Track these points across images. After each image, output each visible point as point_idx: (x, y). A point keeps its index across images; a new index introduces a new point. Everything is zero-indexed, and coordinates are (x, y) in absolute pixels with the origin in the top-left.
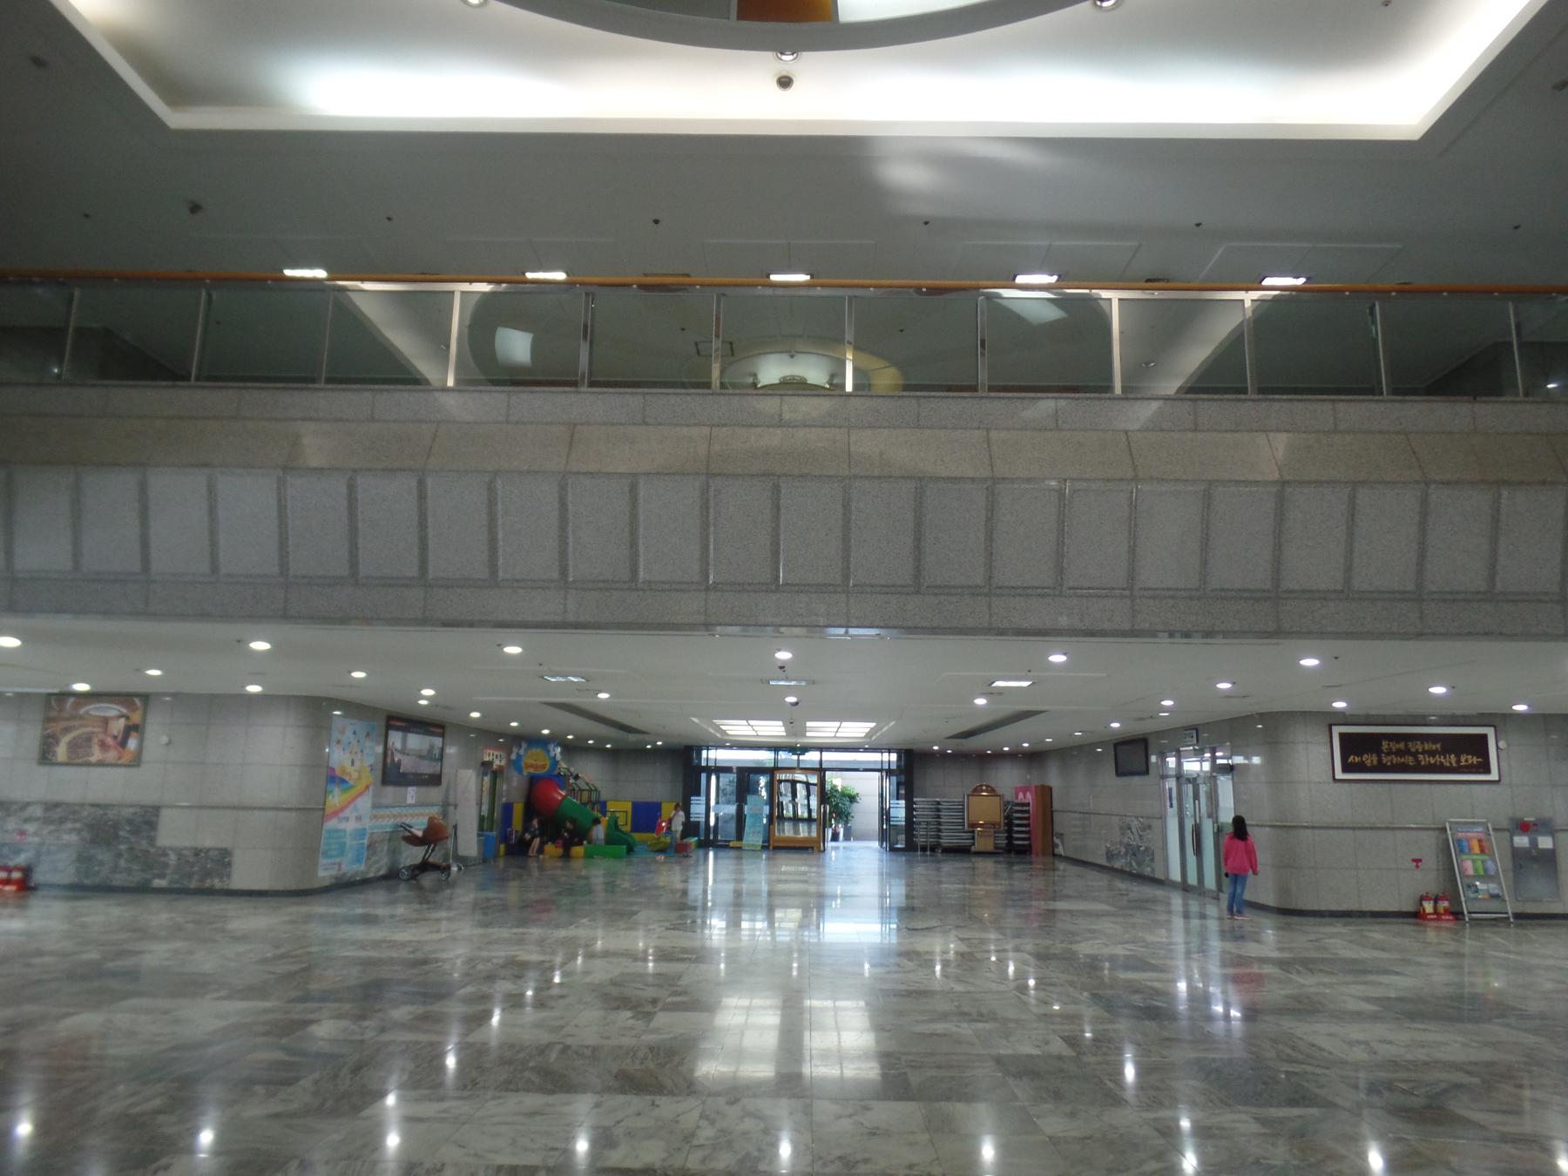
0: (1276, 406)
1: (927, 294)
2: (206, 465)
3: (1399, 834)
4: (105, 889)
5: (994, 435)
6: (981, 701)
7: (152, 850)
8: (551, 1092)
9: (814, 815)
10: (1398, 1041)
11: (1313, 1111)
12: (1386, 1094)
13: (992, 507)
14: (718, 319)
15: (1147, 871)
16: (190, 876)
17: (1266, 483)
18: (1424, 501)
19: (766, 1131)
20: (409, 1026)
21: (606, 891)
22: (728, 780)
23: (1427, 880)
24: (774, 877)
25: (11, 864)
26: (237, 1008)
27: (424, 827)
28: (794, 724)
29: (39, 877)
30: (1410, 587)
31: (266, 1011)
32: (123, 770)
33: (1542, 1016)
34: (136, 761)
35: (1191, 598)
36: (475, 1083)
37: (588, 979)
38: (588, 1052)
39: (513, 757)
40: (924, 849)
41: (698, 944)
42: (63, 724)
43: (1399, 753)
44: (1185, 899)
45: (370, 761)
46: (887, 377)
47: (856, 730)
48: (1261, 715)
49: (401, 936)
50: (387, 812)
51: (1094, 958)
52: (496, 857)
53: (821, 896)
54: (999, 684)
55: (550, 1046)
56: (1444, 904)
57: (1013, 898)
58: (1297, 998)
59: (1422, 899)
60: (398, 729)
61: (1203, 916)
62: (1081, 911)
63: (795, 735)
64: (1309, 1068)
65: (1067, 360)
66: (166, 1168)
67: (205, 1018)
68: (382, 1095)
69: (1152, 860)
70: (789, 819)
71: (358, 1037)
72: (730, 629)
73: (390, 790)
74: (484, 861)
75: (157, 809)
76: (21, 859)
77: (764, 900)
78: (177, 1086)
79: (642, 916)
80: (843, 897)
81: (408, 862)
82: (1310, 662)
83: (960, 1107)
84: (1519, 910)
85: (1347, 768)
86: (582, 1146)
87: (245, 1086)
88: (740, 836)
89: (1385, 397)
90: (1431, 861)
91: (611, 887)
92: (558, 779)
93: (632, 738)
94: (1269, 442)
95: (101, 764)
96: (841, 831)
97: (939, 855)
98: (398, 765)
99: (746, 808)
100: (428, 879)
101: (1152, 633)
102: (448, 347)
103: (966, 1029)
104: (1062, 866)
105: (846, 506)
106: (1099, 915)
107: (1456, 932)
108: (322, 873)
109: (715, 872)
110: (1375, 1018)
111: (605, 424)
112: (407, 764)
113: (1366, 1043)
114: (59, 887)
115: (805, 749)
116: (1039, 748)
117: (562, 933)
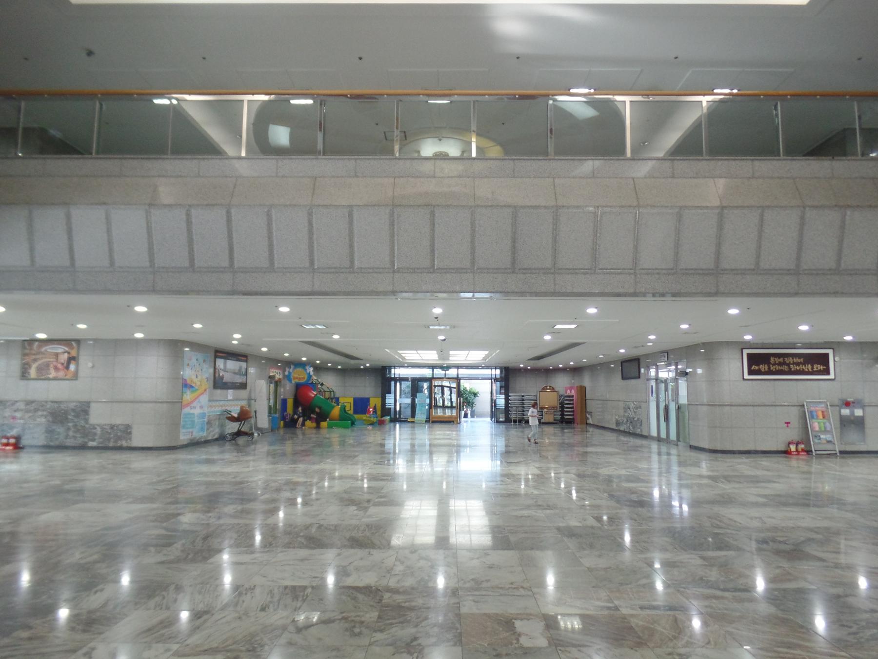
0: (720, 163)
1: (518, 99)
2: (105, 204)
3: (777, 408)
4: (62, 448)
6: (548, 337)
7: (87, 426)
9: (454, 405)
10: (778, 517)
12: (771, 544)
14: (397, 114)
15: (638, 431)
16: (109, 440)
17: (712, 208)
18: (802, 218)
19: (432, 567)
21: (340, 445)
22: (406, 385)
23: (793, 433)
24: (433, 437)
25: (9, 435)
27: (238, 411)
29: (24, 442)
30: (793, 267)
31: (154, 509)
34: (75, 377)
35: (669, 274)
36: (271, 544)
37: (331, 490)
38: (333, 528)
39: (287, 373)
40: (515, 421)
41: (391, 471)
42: (33, 357)
43: (780, 364)
44: (659, 445)
45: (206, 376)
46: (495, 151)
47: (477, 356)
48: (703, 343)
50: (217, 403)
51: (610, 476)
52: (279, 428)
53: (459, 447)
55: (311, 525)
56: (801, 446)
57: (563, 446)
59: (789, 443)
61: (669, 454)
63: (443, 359)
65: (601, 137)
66: (102, 590)
67: (121, 513)
68: (219, 551)
69: (641, 425)
70: (440, 407)
72: (405, 295)
73: (219, 391)
75: (88, 404)
76: (14, 432)
77: (427, 448)
79: (360, 458)
80: (470, 446)
81: (230, 432)
82: (733, 311)
83: (538, 553)
84: (843, 448)
85: (751, 372)
87: (145, 548)
88: (413, 416)
89: (782, 157)
90: (795, 423)
91: (343, 443)
92: (311, 386)
93: (352, 362)
94: (714, 184)
95: (55, 379)
96: (469, 412)
98: (222, 378)
100: (241, 440)
101: (644, 295)
102: (241, 136)
103: (540, 514)
104: (591, 429)
106: (611, 454)
108: (182, 437)
109: (400, 434)
110: (764, 505)
111: (333, 177)
112: (228, 378)
113: (760, 518)
114: (36, 446)
115: (448, 368)
117: (317, 467)
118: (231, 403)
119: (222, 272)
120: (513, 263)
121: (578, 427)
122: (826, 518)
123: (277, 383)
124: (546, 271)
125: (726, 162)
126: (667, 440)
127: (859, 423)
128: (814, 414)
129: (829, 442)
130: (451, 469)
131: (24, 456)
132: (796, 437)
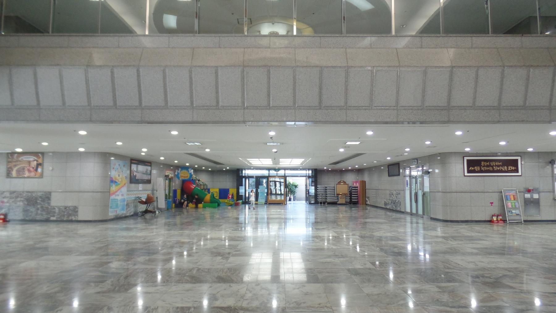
0: (451, 38)
2: (58, 65)
4: (34, 221)
5: (348, 50)
6: (342, 150)
8: (195, 283)
10: (485, 262)
11: (457, 284)
12: (481, 278)
13: (347, 77)
15: (398, 209)
16: (64, 216)
17: (446, 67)
18: (503, 73)
19: (269, 294)
20: (144, 263)
21: (211, 218)
22: (252, 181)
23: (495, 210)
26: (83, 259)
27: (146, 198)
28: (276, 161)
29: (9, 217)
31: (93, 259)
32: (37, 179)
33: (533, 253)
34: (41, 176)
35: (418, 110)
36: (168, 281)
39: (176, 173)
40: (321, 203)
41: (243, 235)
42: (14, 164)
43: (488, 166)
44: (411, 218)
45: (126, 175)
46: (308, 31)
47: (297, 162)
49: (140, 234)
50: (132, 193)
51: (381, 237)
52: (172, 208)
54: (348, 143)
55: (193, 269)
56: (500, 217)
58: (451, 249)
60: (134, 163)
61: (417, 223)
62: (376, 222)
63: (276, 164)
64: (455, 271)
66: (61, 310)
67: (72, 262)
68: (135, 285)
70: (274, 194)
71: (126, 267)
73: (133, 185)
74: (168, 209)
75: (50, 193)
76: (3, 211)
77: (266, 220)
78: (64, 286)
79: (223, 227)
80: (293, 219)
81: (141, 211)
82: (459, 133)
83: (336, 285)
84: (526, 219)
86: (205, 303)
89: (490, 35)
90: (496, 203)
91: (212, 217)
92: (192, 181)
93: (218, 166)
94: (447, 52)
95: (28, 177)
96: (292, 197)
97: (326, 205)
98: (136, 176)
99: (259, 190)
100: (148, 216)
101: (402, 123)
102: (145, 22)
103: (337, 261)
104: (369, 208)
105: (294, 78)
106: (382, 223)
107: (504, 227)
108: (110, 214)
110: (477, 254)
112: (139, 176)
113: (474, 262)
115: (279, 169)
116: (361, 167)
118: (141, 192)
119: (135, 109)
120: (320, 102)
121: (361, 206)
122: (515, 262)
123: (170, 180)
124: (341, 108)
125: (455, 38)
126: (417, 214)
127: (536, 203)
128: (508, 197)
129: (517, 215)
130: (281, 233)
131: (10, 226)
132: (497, 213)
